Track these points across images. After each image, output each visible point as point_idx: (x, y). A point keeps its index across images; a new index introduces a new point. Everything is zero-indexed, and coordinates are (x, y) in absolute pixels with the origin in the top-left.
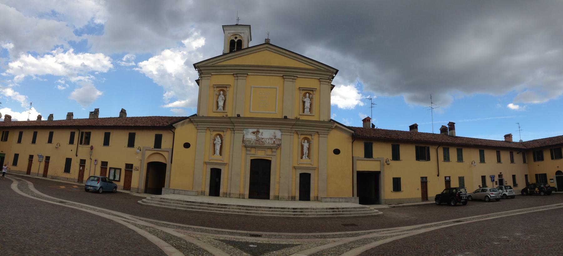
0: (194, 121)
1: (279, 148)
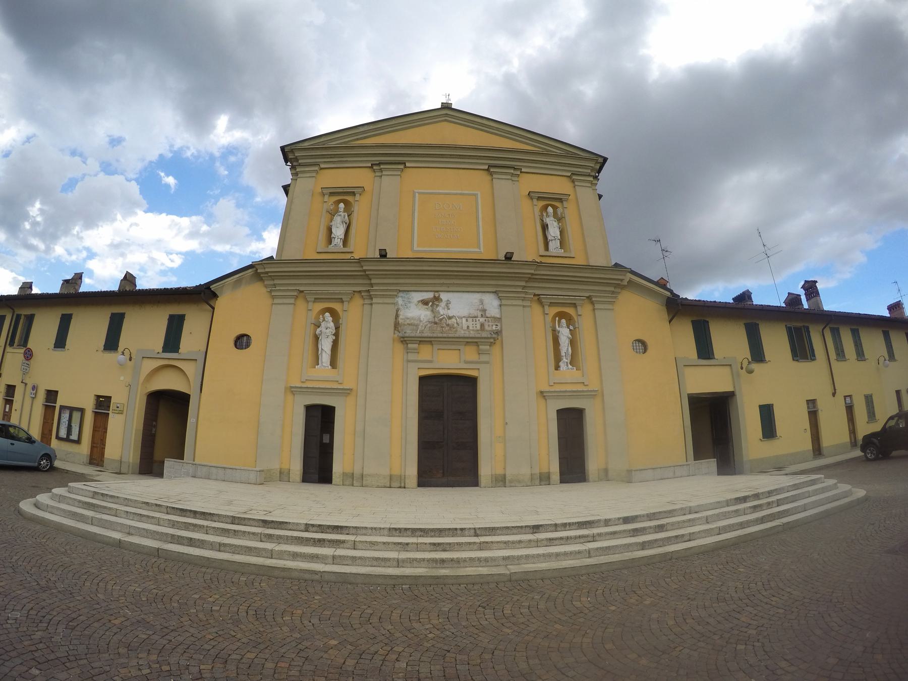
0: (267, 273)
1: (498, 342)
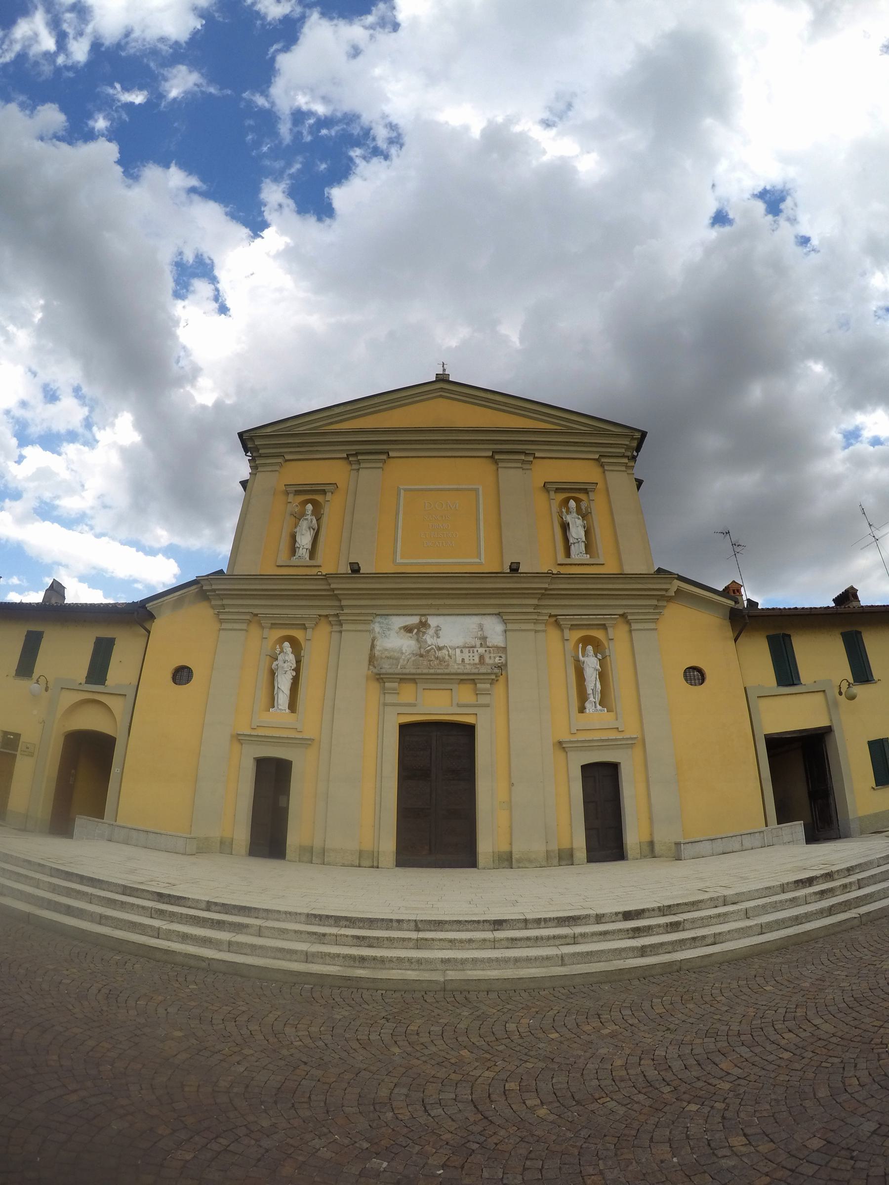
0: (214, 590)
